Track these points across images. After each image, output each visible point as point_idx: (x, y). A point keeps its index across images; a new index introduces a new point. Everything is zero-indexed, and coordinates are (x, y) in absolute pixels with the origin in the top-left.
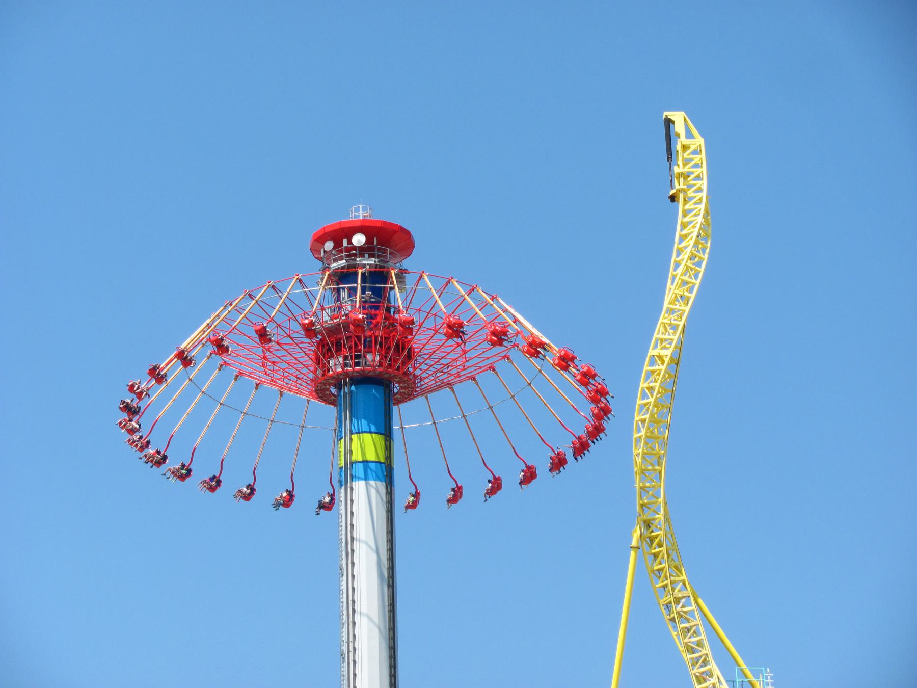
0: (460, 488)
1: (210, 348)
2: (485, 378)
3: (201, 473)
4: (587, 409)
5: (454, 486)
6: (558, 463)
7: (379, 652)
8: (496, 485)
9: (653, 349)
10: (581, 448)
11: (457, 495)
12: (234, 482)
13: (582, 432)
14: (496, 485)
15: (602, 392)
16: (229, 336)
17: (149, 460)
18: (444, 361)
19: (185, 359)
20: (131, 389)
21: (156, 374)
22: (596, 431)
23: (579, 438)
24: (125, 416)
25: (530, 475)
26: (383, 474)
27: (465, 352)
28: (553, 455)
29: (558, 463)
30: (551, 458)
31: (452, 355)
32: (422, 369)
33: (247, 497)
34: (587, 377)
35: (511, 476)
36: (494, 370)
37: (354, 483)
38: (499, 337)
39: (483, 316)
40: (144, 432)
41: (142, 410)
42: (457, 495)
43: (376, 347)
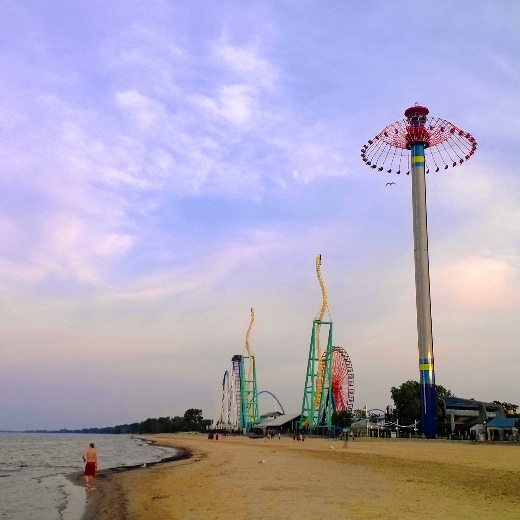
0: (447, 166)
5: (454, 163)
6: (461, 161)
10: (467, 157)
13: (471, 150)
14: (447, 167)
16: (388, 132)
20: (365, 146)
23: (468, 155)
24: (362, 153)
25: (455, 164)
26: (259, 427)
28: (454, 163)
29: (461, 161)
30: (460, 160)
32: (432, 140)
36: (451, 138)
37: (480, 439)
41: (366, 152)
43: (368, 422)
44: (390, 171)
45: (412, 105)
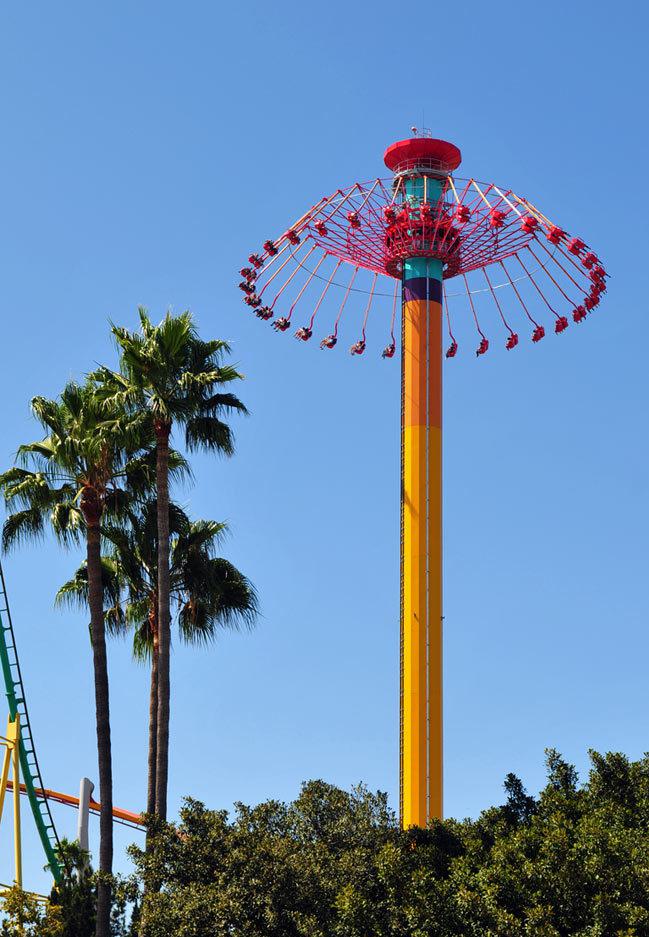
0: (487, 342)
1: (288, 241)
2: (509, 261)
3: (297, 327)
4: (587, 284)
6: (562, 325)
7: (107, 677)
8: (513, 342)
9: (447, 356)
10: (579, 314)
11: (484, 346)
12: (321, 334)
14: (513, 342)
15: (601, 272)
17: (260, 313)
18: (482, 248)
19: (293, 237)
20: (252, 259)
21: (271, 249)
22: (592, 302)
25: (539, 334)
27: (496, 242)
29: (562, 325)
31: (489, 244)
33: (331, 345)
34: (591, 261)
35: (526, 334)
38: (531, 226)
39: (518, 213)
40: (258, 292)
42: (484, 346)
44: (285, 326)
45: (406, 136)
